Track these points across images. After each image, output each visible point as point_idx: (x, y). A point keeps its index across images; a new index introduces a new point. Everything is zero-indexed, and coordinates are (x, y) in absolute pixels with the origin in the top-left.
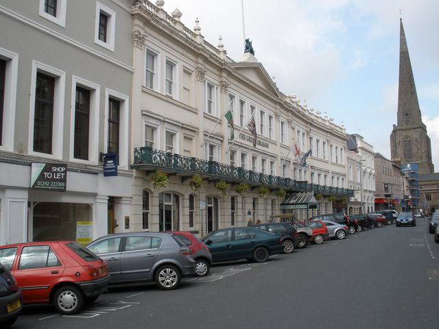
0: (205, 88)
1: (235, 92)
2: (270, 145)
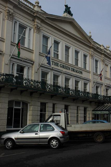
0: (94, 62)
1: (108, 64)
2: (83, 72)
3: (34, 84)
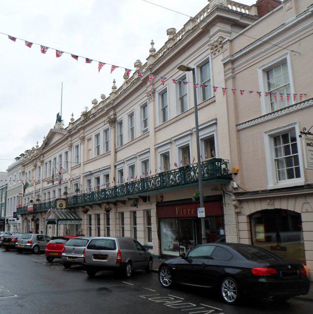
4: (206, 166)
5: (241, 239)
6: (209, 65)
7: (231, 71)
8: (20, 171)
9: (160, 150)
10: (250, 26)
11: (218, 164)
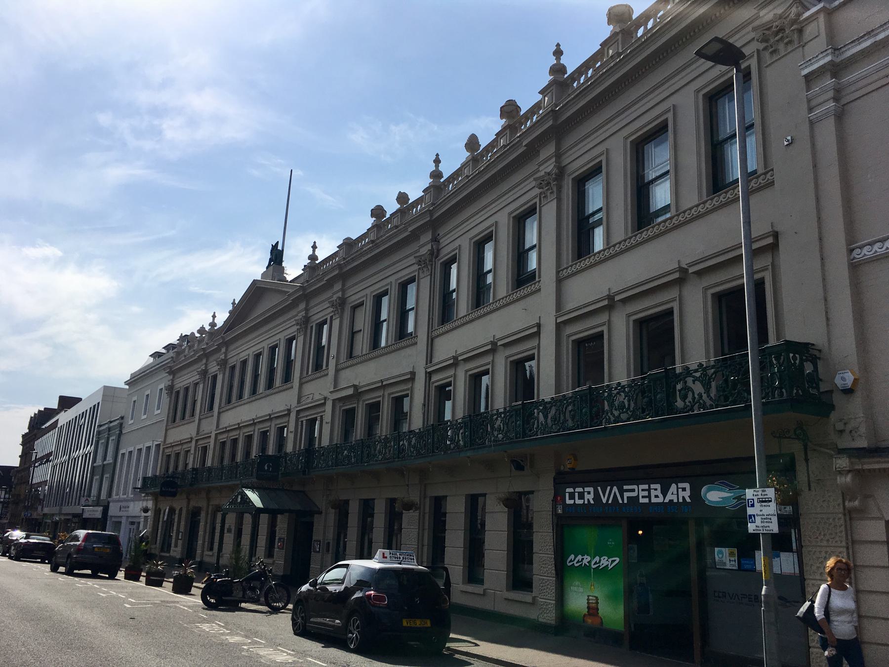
3: (629, 401)
4: (571, 402)
5: (861, 595)
6: (667, 137)
7: (831, 94)
8: (162, 386)
9: (569, 330)
10: (417, 276)
11: (794, 358)
